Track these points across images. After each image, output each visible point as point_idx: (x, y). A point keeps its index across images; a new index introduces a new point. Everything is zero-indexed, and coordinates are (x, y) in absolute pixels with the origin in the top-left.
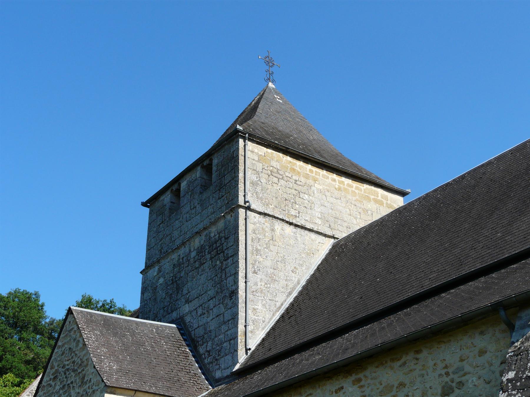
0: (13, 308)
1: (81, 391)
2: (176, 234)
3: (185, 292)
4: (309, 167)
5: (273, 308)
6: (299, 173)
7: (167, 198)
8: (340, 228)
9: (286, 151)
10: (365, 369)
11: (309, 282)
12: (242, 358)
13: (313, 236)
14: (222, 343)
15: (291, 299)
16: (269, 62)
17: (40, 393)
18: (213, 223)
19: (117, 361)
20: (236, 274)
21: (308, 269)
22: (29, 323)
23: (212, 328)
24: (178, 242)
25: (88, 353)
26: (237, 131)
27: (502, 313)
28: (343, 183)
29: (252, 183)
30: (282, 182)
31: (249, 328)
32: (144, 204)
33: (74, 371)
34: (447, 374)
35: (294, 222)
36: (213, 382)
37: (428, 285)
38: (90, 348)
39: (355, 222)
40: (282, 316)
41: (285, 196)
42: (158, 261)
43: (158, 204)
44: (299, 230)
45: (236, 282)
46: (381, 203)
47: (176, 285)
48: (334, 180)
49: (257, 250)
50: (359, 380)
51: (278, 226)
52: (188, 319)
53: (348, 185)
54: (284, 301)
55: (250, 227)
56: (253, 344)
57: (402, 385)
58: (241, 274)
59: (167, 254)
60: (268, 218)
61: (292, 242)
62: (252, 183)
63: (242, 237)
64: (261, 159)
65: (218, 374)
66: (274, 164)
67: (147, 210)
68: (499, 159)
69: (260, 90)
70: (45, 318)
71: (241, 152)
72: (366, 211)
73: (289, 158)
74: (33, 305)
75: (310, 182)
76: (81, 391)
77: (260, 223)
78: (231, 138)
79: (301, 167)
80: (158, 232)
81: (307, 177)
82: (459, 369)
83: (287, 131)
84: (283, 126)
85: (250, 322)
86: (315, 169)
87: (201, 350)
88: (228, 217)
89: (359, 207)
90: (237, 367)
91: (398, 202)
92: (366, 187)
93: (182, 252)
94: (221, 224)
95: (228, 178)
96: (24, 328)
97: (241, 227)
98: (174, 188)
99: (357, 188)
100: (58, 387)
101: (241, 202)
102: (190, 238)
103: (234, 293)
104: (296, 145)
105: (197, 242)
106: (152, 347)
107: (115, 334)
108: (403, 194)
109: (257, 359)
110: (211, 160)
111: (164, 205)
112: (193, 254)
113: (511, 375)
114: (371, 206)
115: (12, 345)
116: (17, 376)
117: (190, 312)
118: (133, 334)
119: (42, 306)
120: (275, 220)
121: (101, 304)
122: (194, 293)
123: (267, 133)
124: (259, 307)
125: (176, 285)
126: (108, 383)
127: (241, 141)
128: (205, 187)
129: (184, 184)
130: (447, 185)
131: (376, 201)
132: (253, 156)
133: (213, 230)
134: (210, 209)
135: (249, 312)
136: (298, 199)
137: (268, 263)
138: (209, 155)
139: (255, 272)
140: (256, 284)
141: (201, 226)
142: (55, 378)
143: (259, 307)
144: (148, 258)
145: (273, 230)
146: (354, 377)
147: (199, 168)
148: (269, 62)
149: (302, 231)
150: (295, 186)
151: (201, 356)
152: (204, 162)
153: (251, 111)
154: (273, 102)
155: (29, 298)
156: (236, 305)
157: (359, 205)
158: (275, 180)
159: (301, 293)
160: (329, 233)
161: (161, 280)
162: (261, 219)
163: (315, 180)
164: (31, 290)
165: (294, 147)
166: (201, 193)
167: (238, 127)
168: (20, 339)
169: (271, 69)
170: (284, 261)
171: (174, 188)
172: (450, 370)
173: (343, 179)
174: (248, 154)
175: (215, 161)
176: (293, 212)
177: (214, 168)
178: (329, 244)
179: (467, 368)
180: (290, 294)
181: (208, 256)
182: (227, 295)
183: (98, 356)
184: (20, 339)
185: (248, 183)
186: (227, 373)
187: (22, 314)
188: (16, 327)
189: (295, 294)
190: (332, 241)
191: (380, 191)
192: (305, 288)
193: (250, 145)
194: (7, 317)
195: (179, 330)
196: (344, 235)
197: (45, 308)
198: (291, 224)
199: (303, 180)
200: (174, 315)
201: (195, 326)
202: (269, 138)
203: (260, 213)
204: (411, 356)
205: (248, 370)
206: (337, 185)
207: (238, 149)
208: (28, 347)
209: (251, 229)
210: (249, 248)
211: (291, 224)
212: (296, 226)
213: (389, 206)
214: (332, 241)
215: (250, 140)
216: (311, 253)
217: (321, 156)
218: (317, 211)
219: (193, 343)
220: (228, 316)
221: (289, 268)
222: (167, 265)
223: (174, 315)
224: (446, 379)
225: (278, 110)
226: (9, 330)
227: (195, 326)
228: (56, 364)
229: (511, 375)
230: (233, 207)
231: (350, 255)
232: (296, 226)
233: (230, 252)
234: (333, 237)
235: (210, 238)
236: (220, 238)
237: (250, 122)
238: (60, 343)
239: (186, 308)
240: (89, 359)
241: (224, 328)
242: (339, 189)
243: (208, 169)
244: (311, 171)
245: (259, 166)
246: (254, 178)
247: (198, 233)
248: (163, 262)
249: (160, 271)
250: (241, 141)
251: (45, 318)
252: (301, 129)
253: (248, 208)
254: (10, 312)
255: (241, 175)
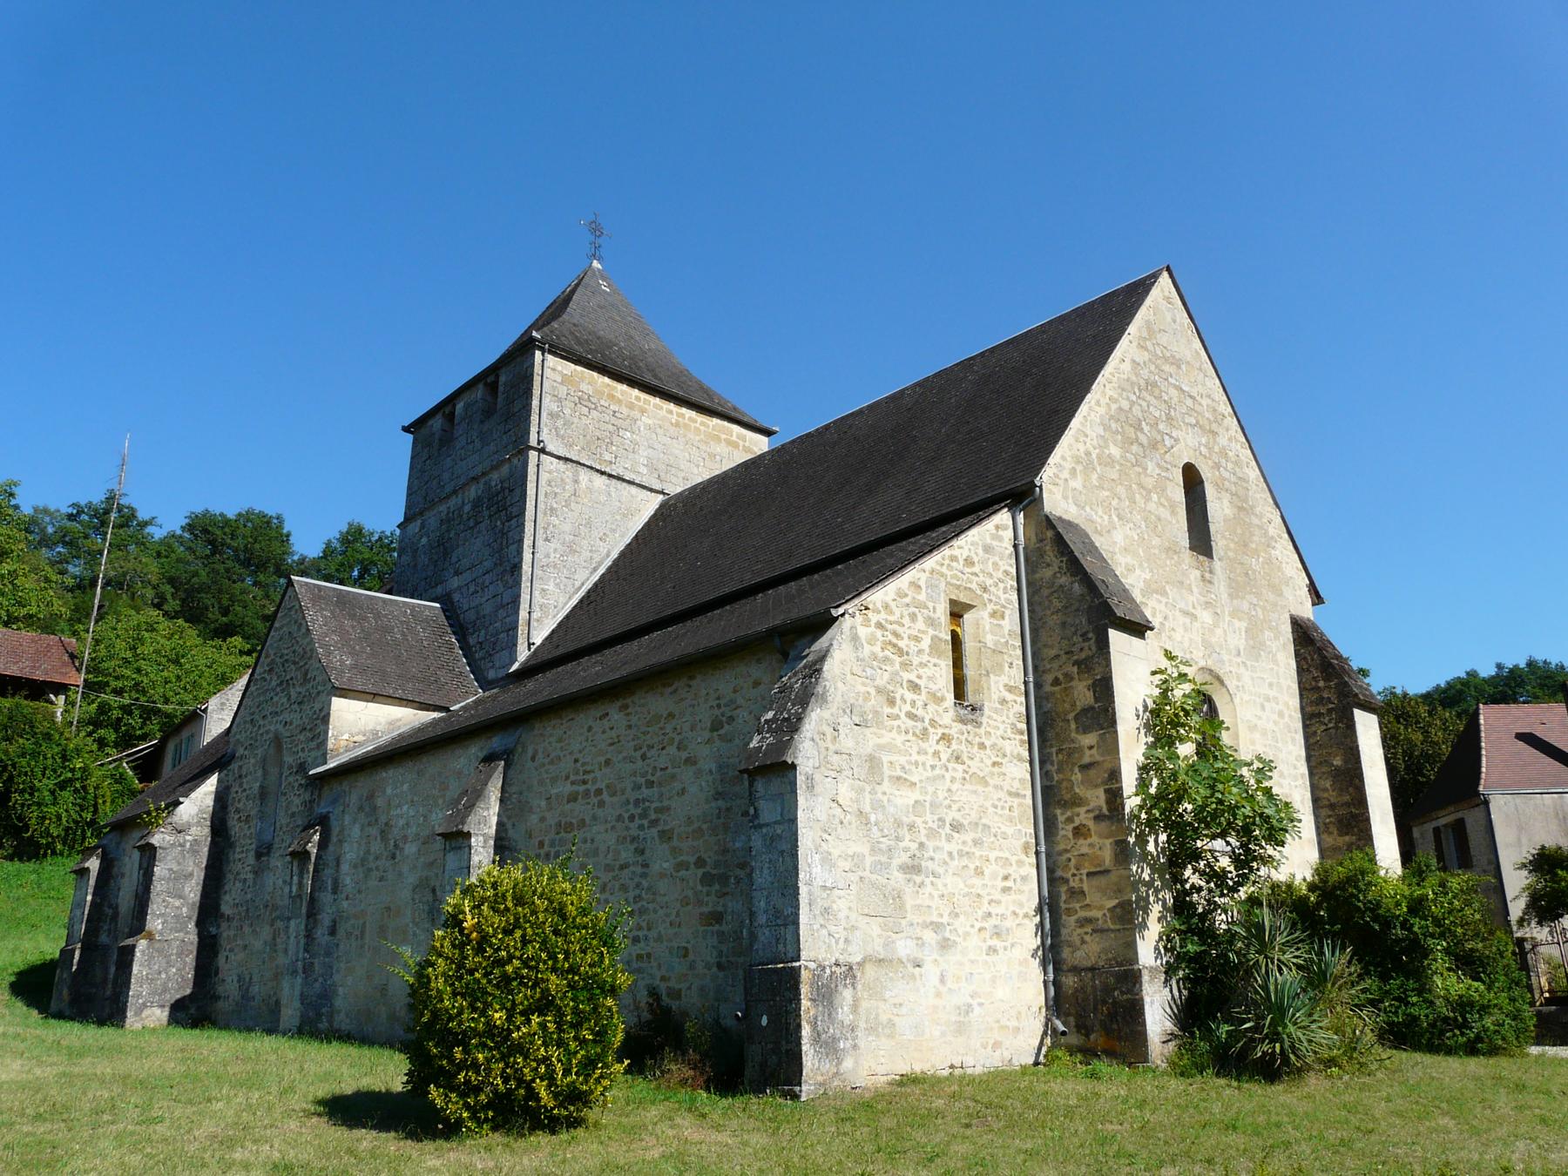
0: (244, 537)
1: (302, 690)
2: (446, 476)
3: (454, 559)
4: (636, 392)
5: (570, 589)
6: (620, 401)
7: (437, 423)
8: (674, 480)
9: (603, 370)
10: (633, 693)
11: (623, 554)
12: (523, 654)
13: (634, 489)
14: (497, 634)
15: (596, 577)
16: (596, 229)
17: (252, 688)
18: (494, 468)
19: (352, 653)
20: (521, 541)
21: (622, 536)
22: (269, 560)
23: (486, 612)
24: (448, 489)
25: (312, 642)
26: (533, 340)
27: (777, 641)
28: (683, 415)
29: (551, 414)
30: (594, 413)
31: (534, 616)
32: (406, 429)
33: (295, 663)
34: (719, 706)
35: (608, 470)
36: (485, 684)
37: (750, 579)
38: (315, 635)
39: (695, 471)
40: (581, 601)
41: (598, 433)
42: (421, 514)
43: (424, 431)
44: (614, 481)
45: (520, 552)
46: (736, 446)
47: (443, 548)
48: (671, 412)
49: (552, 509)
50: (626, 707)
51: (584, 475)
52: (456, 597)
53: (690, 419)
54: (586, 579)
55: (544, 477)
56: (538, 640)
57: (671, 715)
58: (527, 542)
59: (433, 504)
60: (570, 465)
61: (603, 498)
62: (551, 414)
63: (531, 491)
64: (566, 380)
65: (491, 675)
66: (584, 387)
67: (410, 437)
68: (871, 407)
69: (579, 272)
70: (292, 554)
71: (537, 369)
72: (712, 456)
73: (606, 380)
74: (274, 534)
75: (636, 414)
76: (302, 690)
77: (558, 471)
78: (523, 349)
79: (623, 393)
80: (423, 471)
81: (631, 406)
82: (732, 701)
83: (612, 337)
84: (606, 328)
85: (536, 608)
86: (643, 396)
87: (472, 641)
88: (515, 461)
89: (704, 450)
90: (515, 667)
91: (761, 444)
92: (716, 421)
93: (453, 502)
94: (505, 469)
95: (517, 406)
96: (262, 566)
97: (531, 477)
98: (447, 410)
99: (702, 424)
100: (274, 683)
101: (533, 441)
102: (465, 485)
103: (516, 568)
104: (619, 361)
105: (473, 492)
106: (403, 634)
107: (352, 617)
108: (767, 433)
109: (547, 656)
110: (497, 376)
111: (435, 432)
112: (467, 508)
113: (770, 715)
114: (721, 449)
115: (243, 592)
116: (246, 638)
117: (460, 588)
118: (378, 616)
119: (288, 535)
120: (580, 468)
121: (376, 537)
122: (465, 562)
123: (579, 342)
124: (551, 587)
125: (443, 548)
126: (337, 684)
127: (538, 354)
128: (488, 413)
129: (460, 406)
130: (809, 435)
131: (729, 443)
132: (552, 371)
133: (495, 476)
134: (492, 447)
135: (536, 593)
136: (615, 439)
137: (567, 527)
138: (494, 369)
139: (547, 540)
140: (548, 556)
141: (478, 471)
142: (271, 670)
143: (551, 587)
144: (408, 507)
145: (576, 481)
146: (619, 704)
147: (481, 386)
148: (596, 229)
149: (619, 483)
150: (613, 420)
151: (470, 648)
152: (488, 378)
153: (559, 307)
154: (596, 291)
155: (268, 523)
156: (518, 584)
157: (703, 447)
158: (585, 410)
159: (609, 569)
160: (658, 487)
161: (424, 540)
162: (561, 465)
163: (643, 411)
164: (271, 512)
165: (615, 363)
166: (482, 422)
167: (534, 334)
168: (255, 584)
169: (598, 241)
170: (589, 524)
171: (447, 410)
172: (722, 702)
173: (684, 410)
174: (547, 372)
175: (502, 379)
176: (607, 457)
177: (501, 388)
178: (652, 504)
179: (740, 701)
180: (595, 569)
181: (486, 513)
182: (509, 569)
183: (325, 646)
184: (255, 584)
185: (544, 414)
186: (501, 673)
187: (257, 546)
188: (249, 565)
189: (602, 571)
190: (661, 498)
191: (736, 428)
192: (616, 562)
193: (551, 360)
194: (236, 550)
195: (444, 611)
196: (679, 490)
197: (292, 540)
198: (603, 473)
199: (625, 410)
200: (439, 590)
201: (466, 607)
202: (579, 349)
203: (559, 458)
204: (685, 680)
205: (528, 671)
206: (674, 419)
207: (533, 365)
208: (267, 596)
209: (546, 481)
210: (541, 506)
211: (603, 473)
212: (610, 476)
213: (747, 450)
214: (661, 498)
215: (550, 352)
216: (628, 514)
217: (655, 376)
218: (643, 455)
219: (461, 630)
220: (507, 598)
221: (596, 534)
222: (432, 518)
223: (439, 590)
224: (717, 712)
225: (615, 295)
226: (238, 569)
227: (466, 607)
228: (272, 652)
229: (770, 715)
230: (522, 448)
231: (684, 521)
232: (610, 476)
233: (515, 510)
234: (662, 493)
235: (490, 487)
236: (503, 489)
237: (555, 325)
238: (277, 625)
239: (455, 582)
240: (313, 650)
241: (502, 613)
242: (677, 425)
243: (493, 388)
244: (638, 399)
245: (563, 391)
246: (554, 407)
247: (475, 479)
248: (427, 514)
249: (423, 526)
250: (538, 354)
251: (292, 554)
252: (633, 332)
253: (542, 451)
254: (239, 543)
255: (535, 403)
